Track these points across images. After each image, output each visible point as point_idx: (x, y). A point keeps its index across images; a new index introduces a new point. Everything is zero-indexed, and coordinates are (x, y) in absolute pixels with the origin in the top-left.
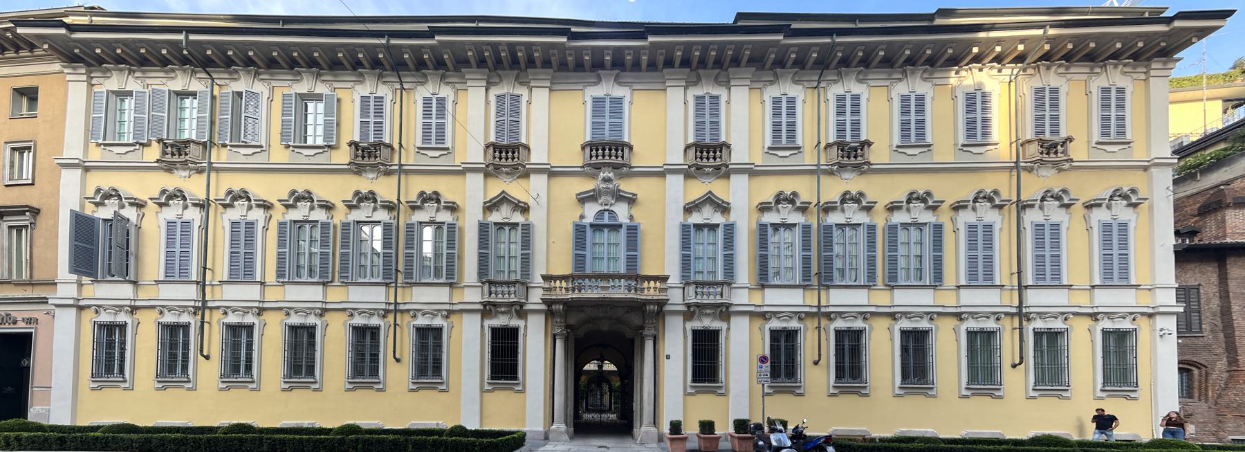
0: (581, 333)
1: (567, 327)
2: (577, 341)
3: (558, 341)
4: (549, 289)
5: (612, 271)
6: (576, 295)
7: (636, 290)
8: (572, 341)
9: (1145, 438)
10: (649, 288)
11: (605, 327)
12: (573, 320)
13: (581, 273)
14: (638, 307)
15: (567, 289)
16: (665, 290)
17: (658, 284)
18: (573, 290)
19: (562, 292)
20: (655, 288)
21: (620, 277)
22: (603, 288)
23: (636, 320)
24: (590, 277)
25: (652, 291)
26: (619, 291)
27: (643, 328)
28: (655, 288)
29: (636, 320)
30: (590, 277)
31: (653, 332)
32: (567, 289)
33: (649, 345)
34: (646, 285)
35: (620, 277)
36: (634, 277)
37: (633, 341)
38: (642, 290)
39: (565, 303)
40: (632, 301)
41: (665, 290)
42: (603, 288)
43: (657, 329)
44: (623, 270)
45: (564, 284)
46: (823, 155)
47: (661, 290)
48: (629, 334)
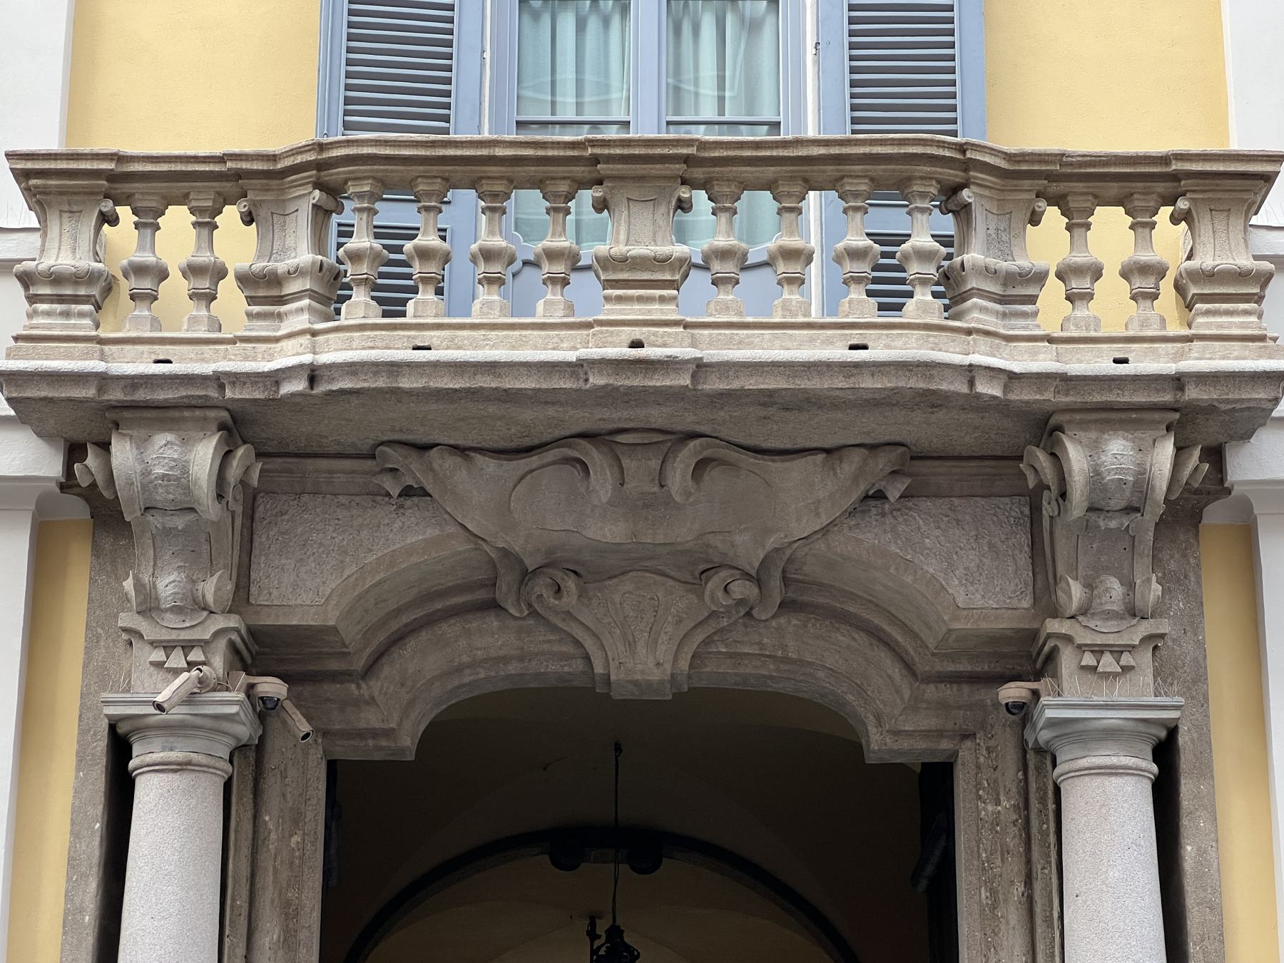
0: (393, 715)
1: (258, 651)
2: (354, 792)
3: (150, 794)
4: (88, 290)
5: (709, 110)
6: (354, 342)
7: (952, 288)
8: (300, 791)
9: (1099, 210)
10: (1079, 278)
11: (643, 649)
12: (314, 583)
13: (405, 137)
14: (996, 452)
15: (264, 288)
16: (1248, 286)
17: (1169, 239)
18: (331, 290)
19: (217, 315)
20: (206, 276)
21: (791, 170)
22: (623, 274)
23: (958, 576)
24: (492, 173)
25: (1112, 305)
26: (786, 305)
27: (1035, 660)
28: (1143, 275)
29: (958, 576)
30: (492, 173)
31: (1140, 695)
32: (264, 288)
33: (1107, 823)
34: (1048, 240)
35: (791, 170)
36: (922, 165)
37: (935, 783)
38: (1018, 290)
39: (241, 417)
40: (920, 392)
41: (1248, 286)
42: (623, 274)
43: (1175, 665)
44: (813, 110)
45: (236, 242)
46: (1049, 475)
47: (1200, 289)
48: (894, 727)
